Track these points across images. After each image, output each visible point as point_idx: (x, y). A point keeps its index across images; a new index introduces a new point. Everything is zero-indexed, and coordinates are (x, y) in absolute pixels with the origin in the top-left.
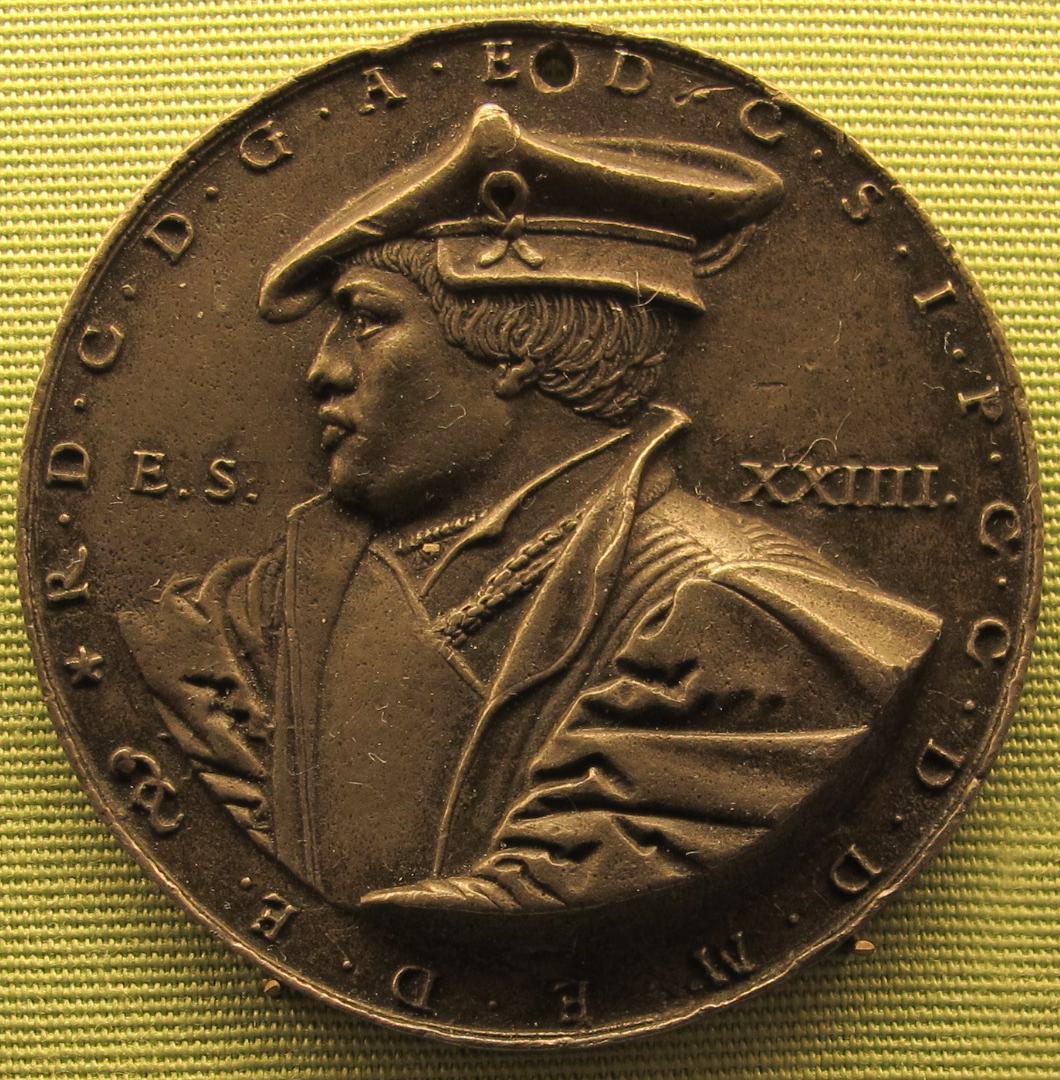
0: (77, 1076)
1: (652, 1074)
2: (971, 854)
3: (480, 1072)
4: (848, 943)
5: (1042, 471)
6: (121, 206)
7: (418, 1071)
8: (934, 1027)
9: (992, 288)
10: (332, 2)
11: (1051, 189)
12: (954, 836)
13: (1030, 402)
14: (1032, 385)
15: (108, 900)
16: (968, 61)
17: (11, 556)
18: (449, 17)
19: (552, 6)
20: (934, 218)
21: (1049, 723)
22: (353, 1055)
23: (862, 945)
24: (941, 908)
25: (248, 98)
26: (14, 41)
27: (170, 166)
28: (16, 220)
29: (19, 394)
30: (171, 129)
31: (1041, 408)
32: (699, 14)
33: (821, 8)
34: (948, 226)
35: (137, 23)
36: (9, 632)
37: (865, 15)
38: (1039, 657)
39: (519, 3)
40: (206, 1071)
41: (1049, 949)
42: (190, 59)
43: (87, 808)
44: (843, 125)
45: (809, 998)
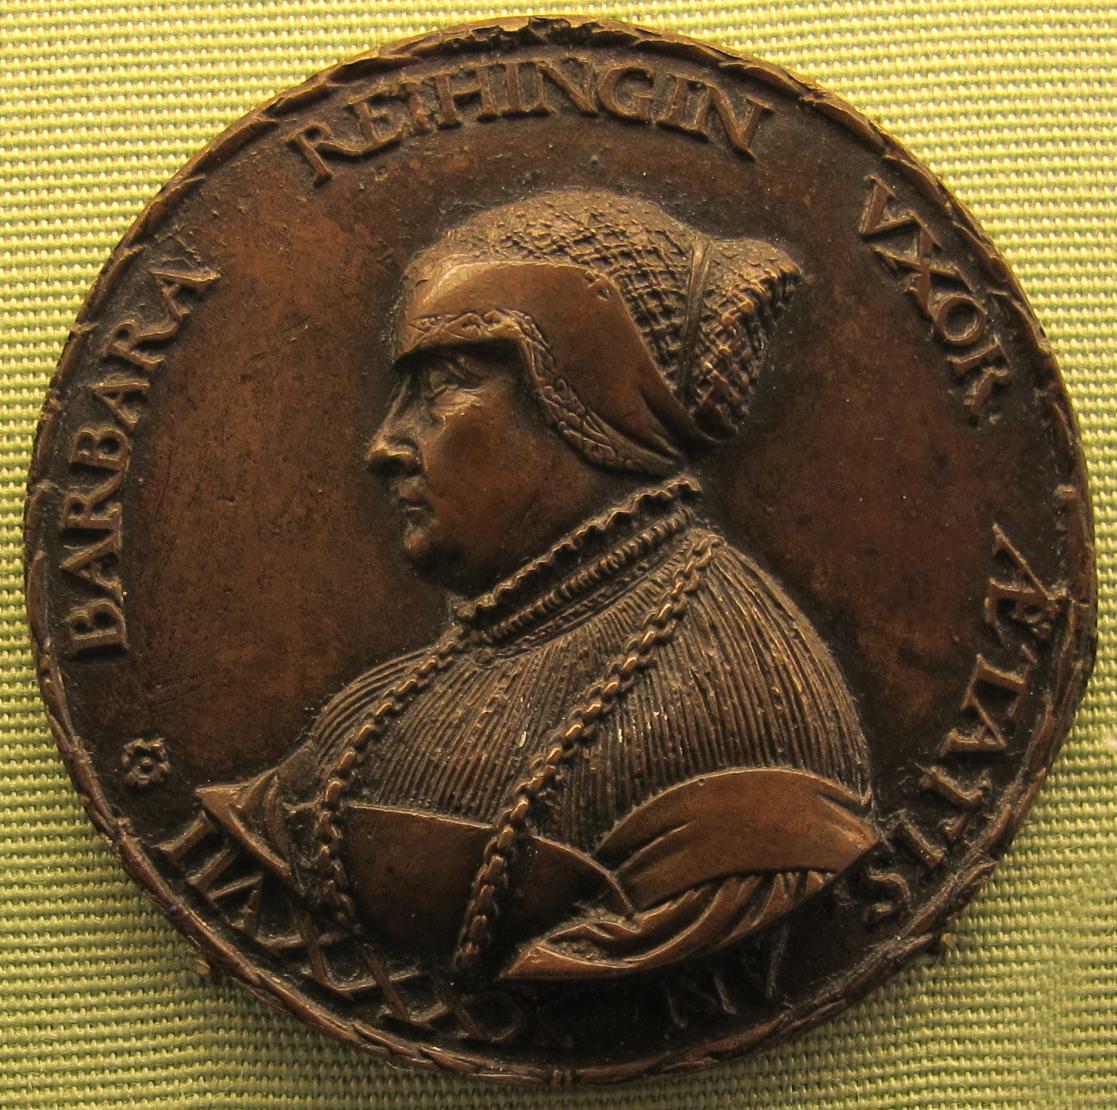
2: (1004, 974)
3: (476, 1101)
7: (411, 1100)
10: (447, 2)
15: (59, 860)
18: (421, 25)
19: (631, 8)
20: (976, 210)
21: (1105, 802)
29: (30, 388)
32: (122, 13)
33: (114, 8)
34: (991, 219)
35: (129, 58)
37: (72, 16)
38: (1105, 576)
39: (620, 3)
44: (903, 136)
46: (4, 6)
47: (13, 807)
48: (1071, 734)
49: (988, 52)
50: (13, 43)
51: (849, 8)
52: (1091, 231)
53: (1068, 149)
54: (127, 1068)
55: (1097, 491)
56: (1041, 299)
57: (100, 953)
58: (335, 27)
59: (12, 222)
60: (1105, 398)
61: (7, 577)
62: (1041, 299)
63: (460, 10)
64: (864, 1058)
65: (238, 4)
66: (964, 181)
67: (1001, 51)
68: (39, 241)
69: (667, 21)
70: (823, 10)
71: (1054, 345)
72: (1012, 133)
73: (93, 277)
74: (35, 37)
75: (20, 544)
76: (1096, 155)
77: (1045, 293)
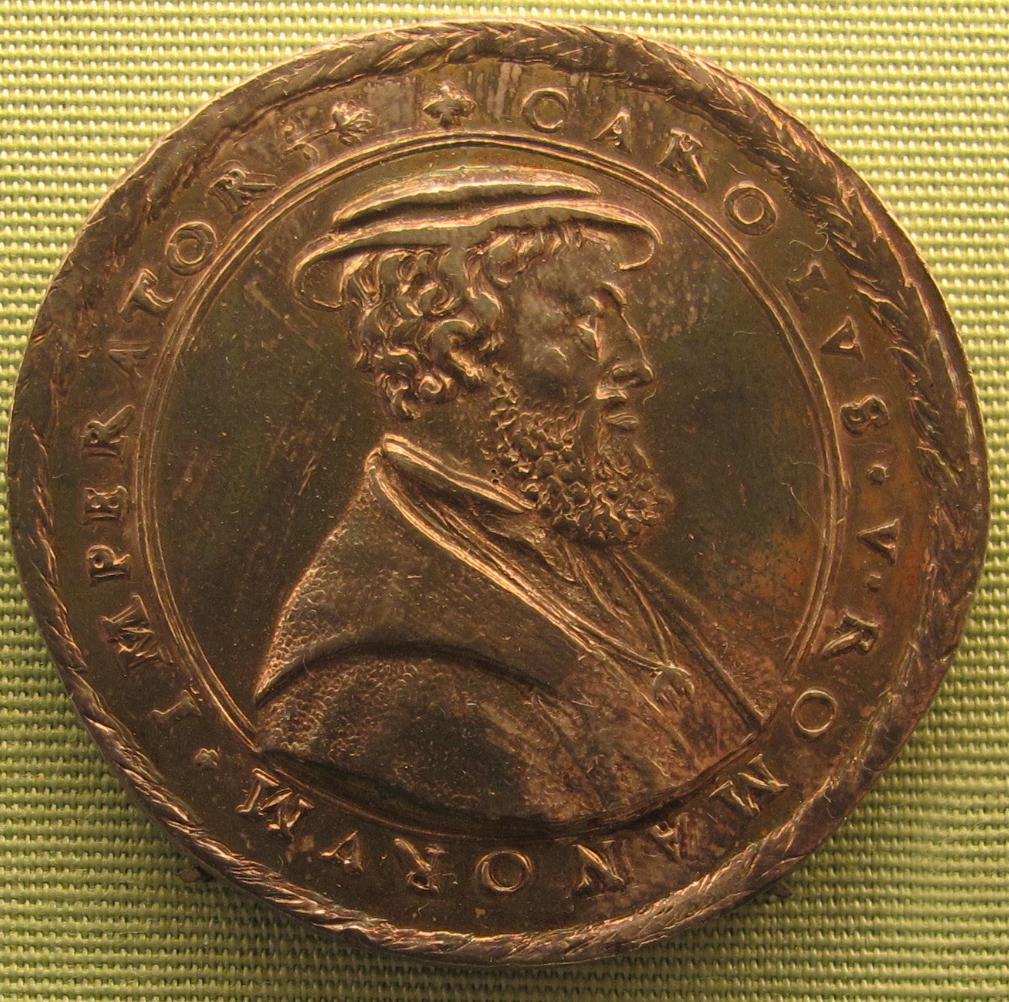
5: (994, 493)
6: (187, 112)
8: (921, 813)
13: (986, 419)
14: (987, 401)
16: (948, 57)
24: (870, 827)
25: (272, 61)
27: (112, 191)
30: (192, 61)
36: (10, 761)
39: (261, 2)
41: (998, 964)
42: (174, 49)
43: (31, 619)
46: (6, 6)
47: (13, 883)
48: (900, 754)
49: (844, 33)
52: (921, 184)
53: (936, 134)
57: (98, 971)
63: (566, 8)
64: (803, 971)
65: (782, 4)
67: (907, 35)
68: (18, 65)
70: (144, 7)
72: (930, 116)
73: (81, 225)
74: (60, 192)
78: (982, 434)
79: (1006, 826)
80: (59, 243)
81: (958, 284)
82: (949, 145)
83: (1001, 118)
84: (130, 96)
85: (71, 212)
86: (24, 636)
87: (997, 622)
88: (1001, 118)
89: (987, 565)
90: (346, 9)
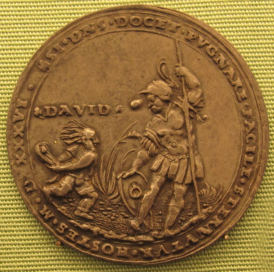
0: (43, 271)
1: (153, 271)
4: (223, 236)
9: (254, 71)
11: (272, 70)
12: (247, 211)
17: (5, 130)
22: (88, 261)
23: (226, 237)
26: (4, 87)
28: (4, 11)
31: (3, 269)
32: (31, 4)
36: (3, 263)
38: (270, 164)
39: (268, 1)
40: (67, 269)
45: (217, 250)
50: (10, 33)
51: (74, 3)
54: (8, 262)
55: (265, 96)
56: (248, 59)
58: (72, 5)
59: (4, 245)
60: (270, 78)
61: (2, 223)
62: (248, 59)
66: (231, 38)
69: (154, 4)
71: (250, 68)
75: (6, 125)
76: (265, 17)
77: (249, 57)
78: (122, 256)
79: (273, 252)
80: (26, 58)
81: (212, 21)
82: (261, 19)
83: (272, 11)
84: (21, 13)
85: (28, 53)
86: (10, 184)
87: (245, 248)
88: (272, 11)
89: (269, 156)
90: (64, 3)
